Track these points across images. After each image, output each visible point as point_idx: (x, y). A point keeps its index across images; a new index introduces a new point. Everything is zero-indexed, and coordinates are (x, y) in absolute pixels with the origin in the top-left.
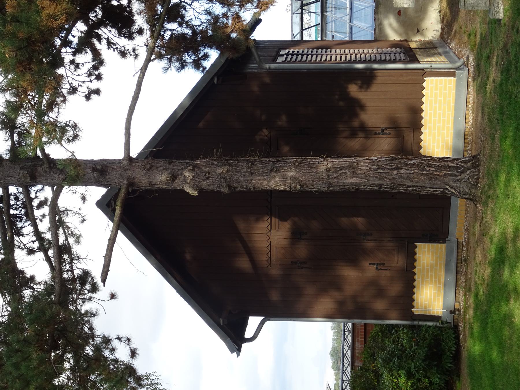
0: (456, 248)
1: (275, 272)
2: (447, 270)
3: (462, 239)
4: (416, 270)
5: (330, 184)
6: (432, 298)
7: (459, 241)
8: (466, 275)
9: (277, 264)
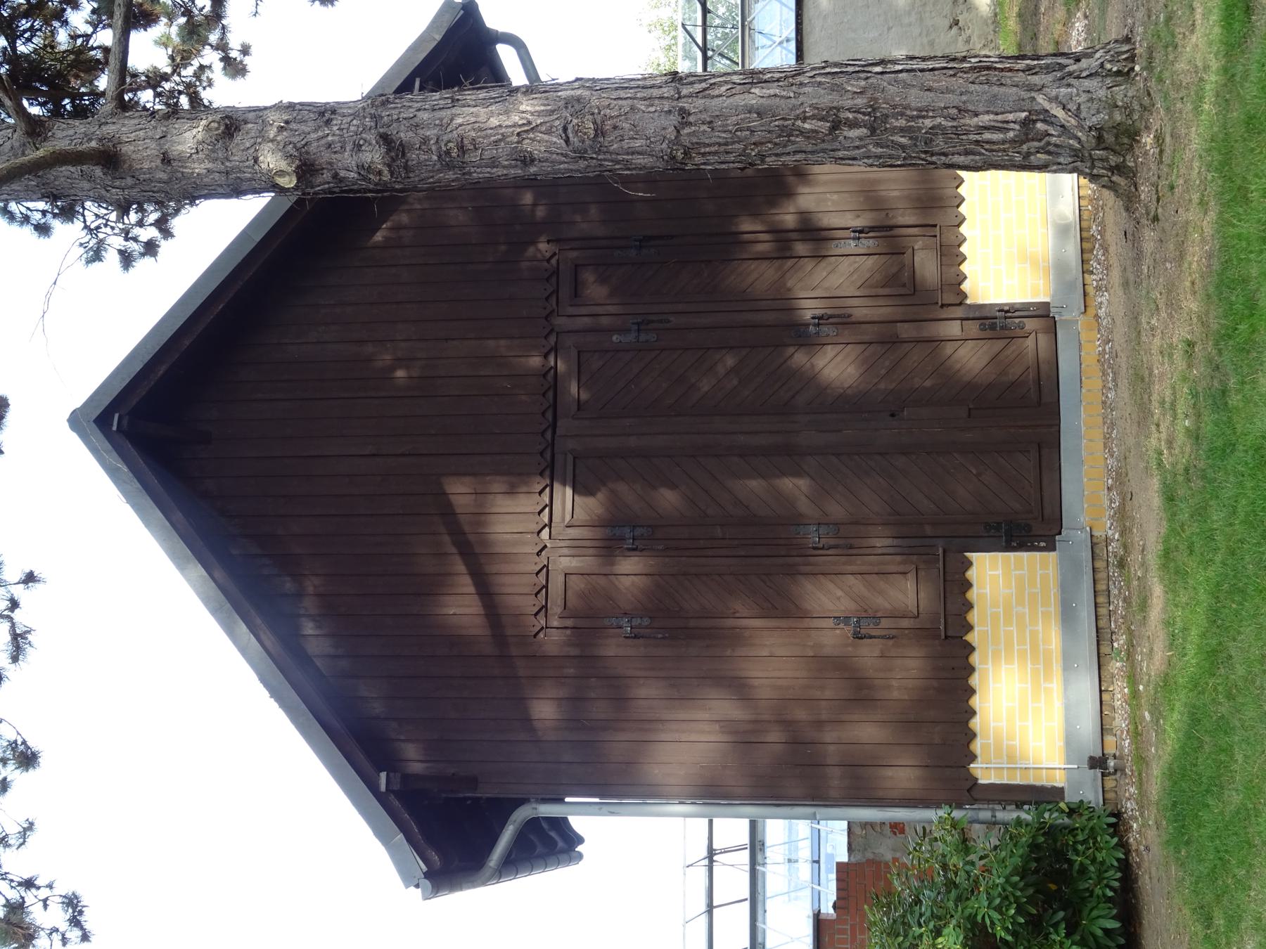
0: (1087, 555)
1: (554, 640)
2: (1067, 616)
3: (1106, 528)
4: (973, 638)
5: (683, 113)
6: (1032, 713)
7: (1096, 533)
8: (1130, 656)
9: (566, 628)
